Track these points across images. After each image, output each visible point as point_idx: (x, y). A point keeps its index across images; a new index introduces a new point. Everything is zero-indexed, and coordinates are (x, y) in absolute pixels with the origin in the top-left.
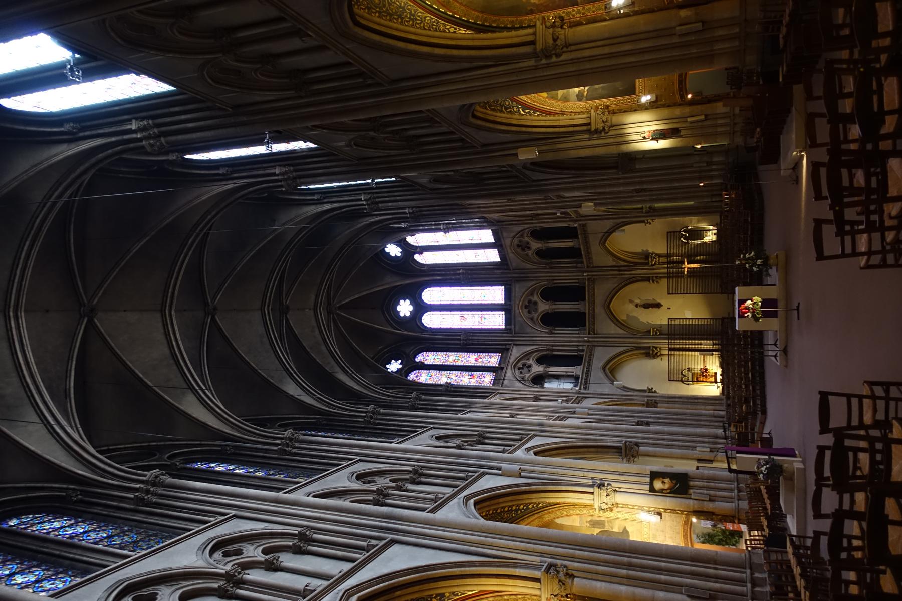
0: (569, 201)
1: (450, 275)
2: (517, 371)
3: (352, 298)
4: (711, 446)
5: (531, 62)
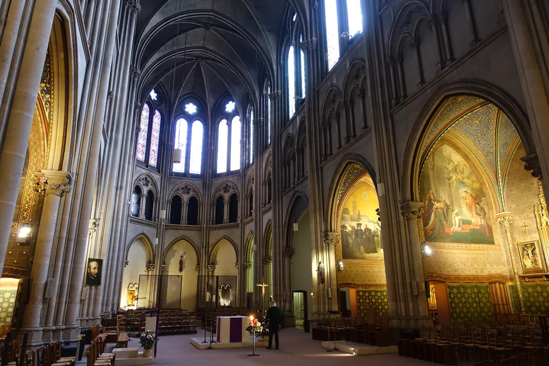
0: (260, 218)
1: (211, 140)
3: (203, 74)
5: (399, 198)
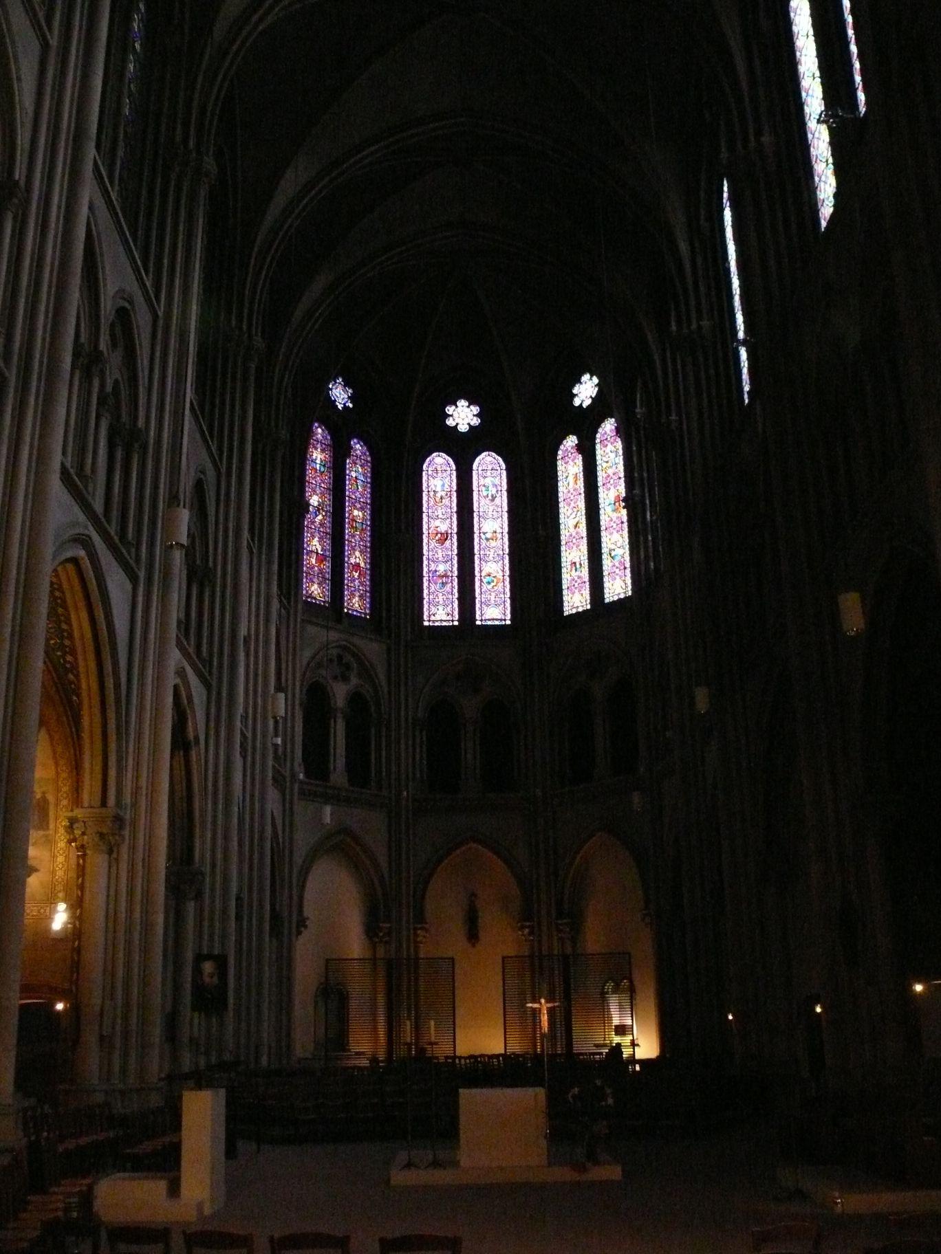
2: (335, 652)
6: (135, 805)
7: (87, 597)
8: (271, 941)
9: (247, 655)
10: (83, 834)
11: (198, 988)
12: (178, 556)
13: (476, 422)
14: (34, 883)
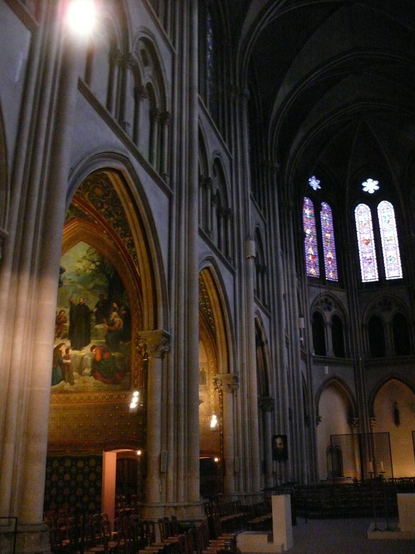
2: (323, 298)
4: (278, 473)
6: (242, 371)
7: (215, 285)
8: (305, 428)
9: (285, 302)
10: (221, 385)
11: (275, 451)
12: (251, 262)
13: (377, 188)
14: (202, 407)
